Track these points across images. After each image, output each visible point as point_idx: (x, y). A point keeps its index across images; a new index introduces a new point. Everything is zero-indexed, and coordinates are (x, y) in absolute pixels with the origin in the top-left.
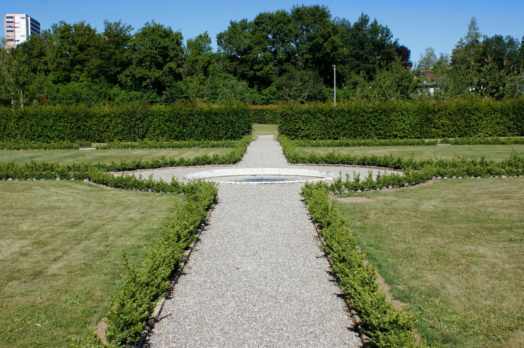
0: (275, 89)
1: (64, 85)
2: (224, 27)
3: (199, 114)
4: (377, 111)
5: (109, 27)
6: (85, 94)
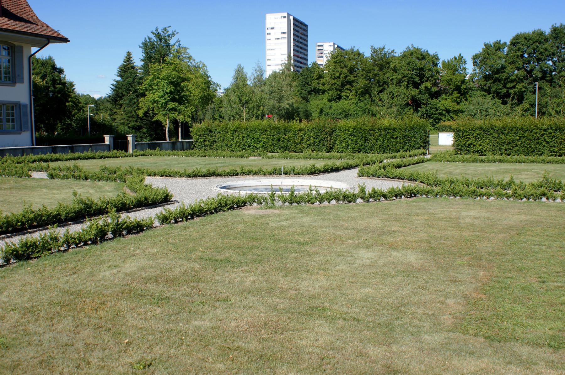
0: (529, 106)
1: (336, 102)
2: (479, 49)
3: (379, 129)
4: (551, 128)
5: (375, 51)
6: (352, 110)
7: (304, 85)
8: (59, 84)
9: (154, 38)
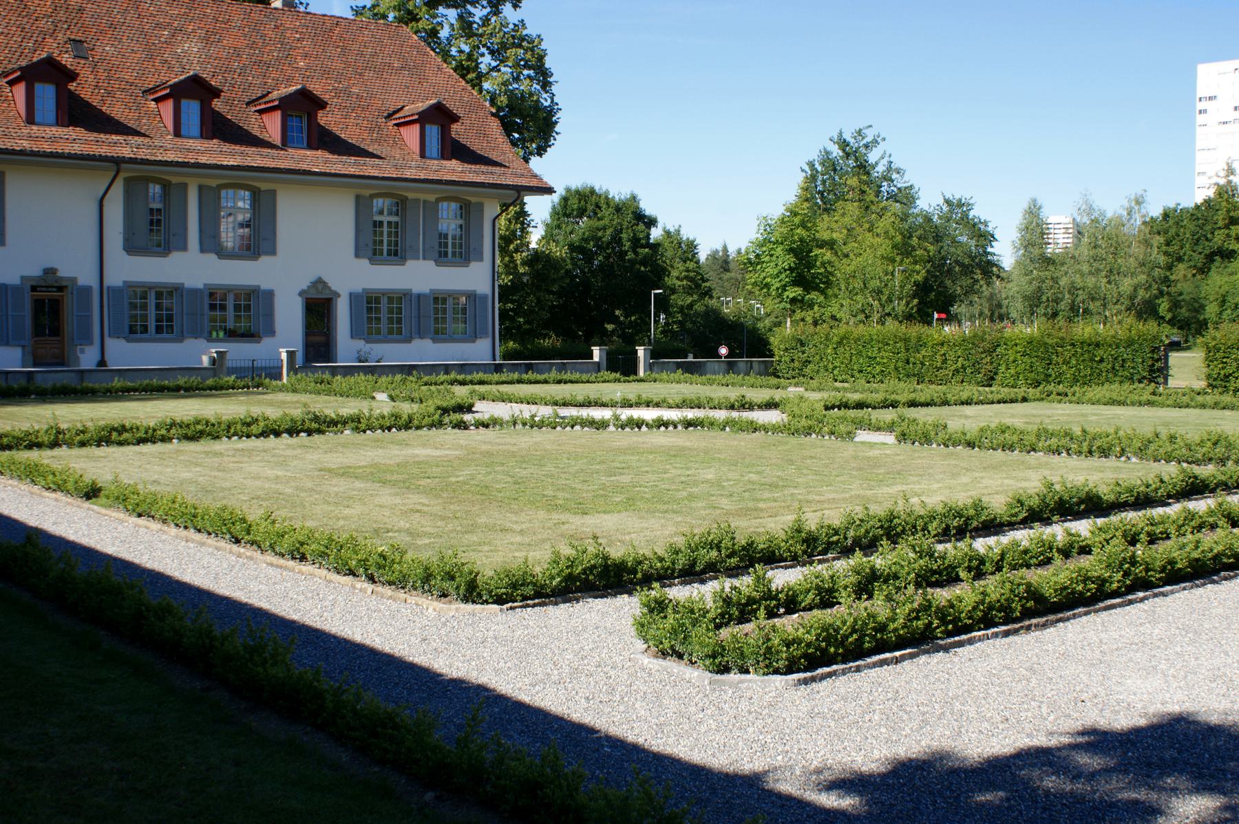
3: (1073, 345)
7: (1198, 240)
8: (643, 246)
9: (836, 151)
